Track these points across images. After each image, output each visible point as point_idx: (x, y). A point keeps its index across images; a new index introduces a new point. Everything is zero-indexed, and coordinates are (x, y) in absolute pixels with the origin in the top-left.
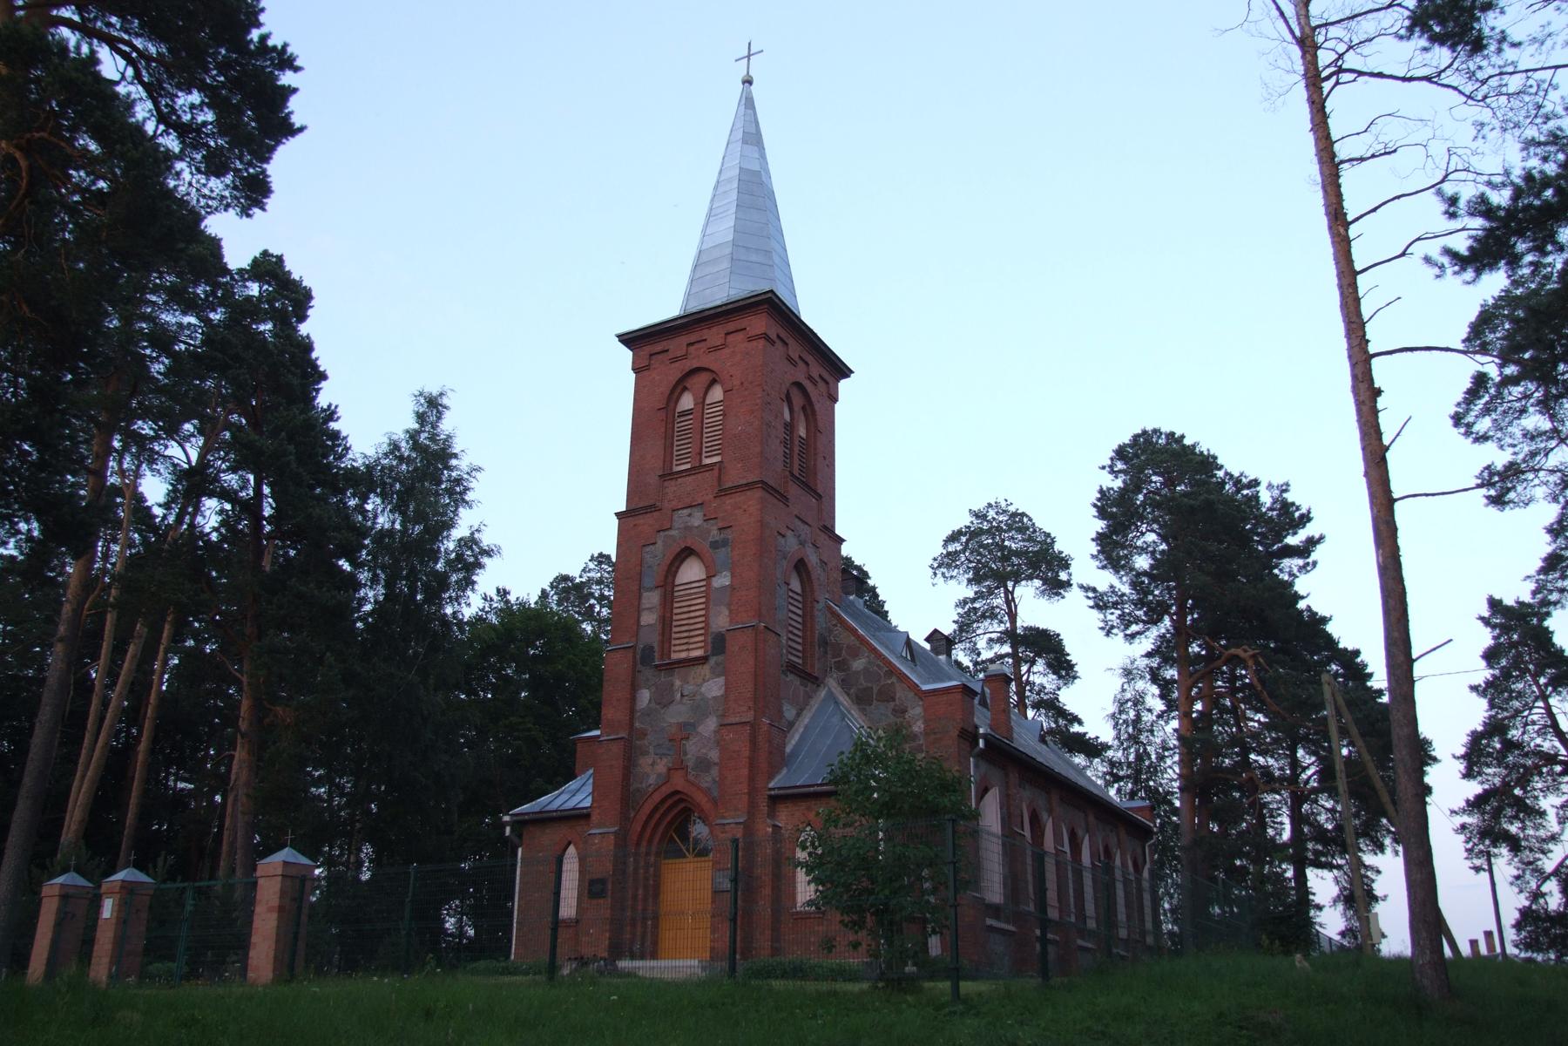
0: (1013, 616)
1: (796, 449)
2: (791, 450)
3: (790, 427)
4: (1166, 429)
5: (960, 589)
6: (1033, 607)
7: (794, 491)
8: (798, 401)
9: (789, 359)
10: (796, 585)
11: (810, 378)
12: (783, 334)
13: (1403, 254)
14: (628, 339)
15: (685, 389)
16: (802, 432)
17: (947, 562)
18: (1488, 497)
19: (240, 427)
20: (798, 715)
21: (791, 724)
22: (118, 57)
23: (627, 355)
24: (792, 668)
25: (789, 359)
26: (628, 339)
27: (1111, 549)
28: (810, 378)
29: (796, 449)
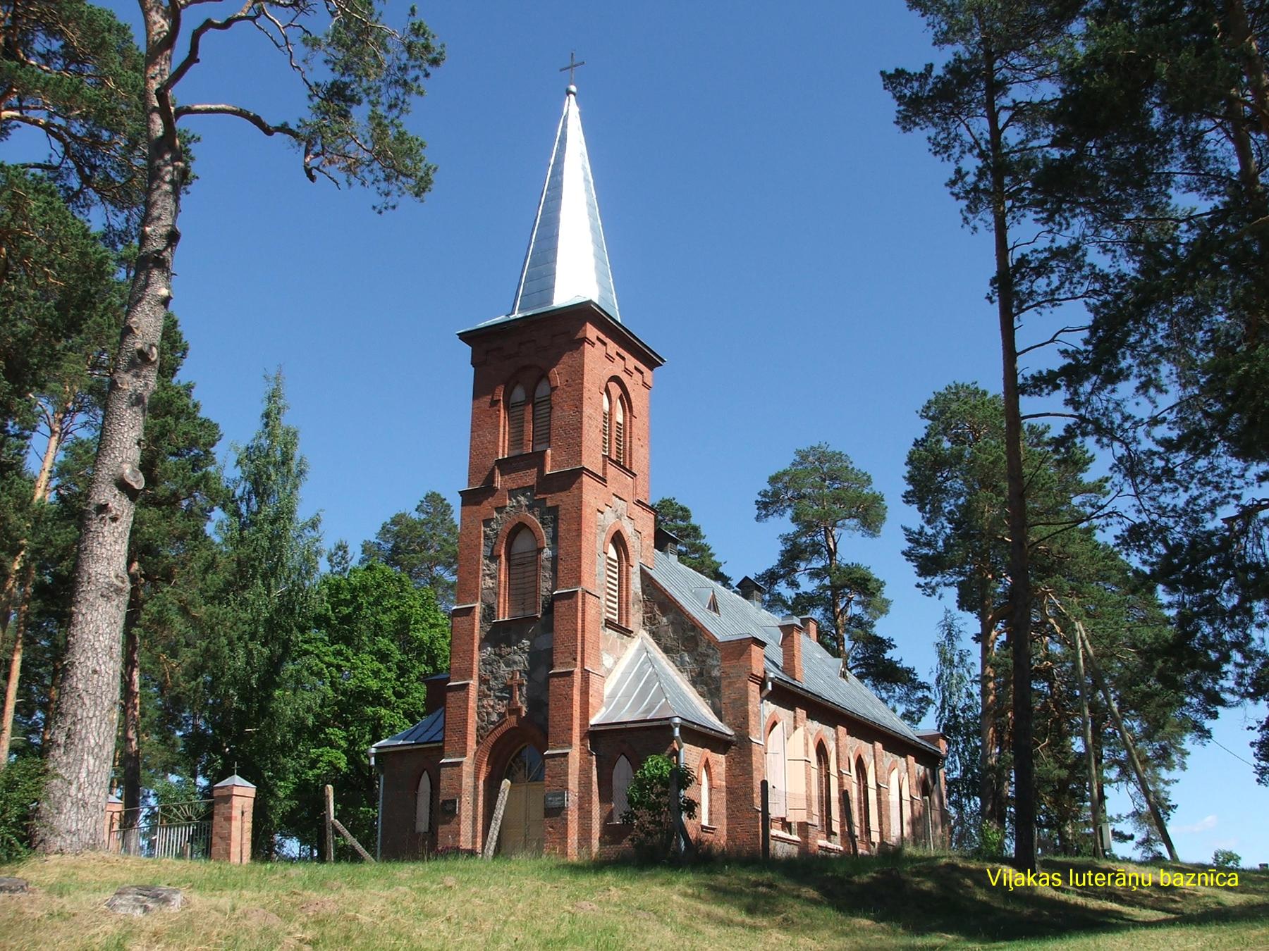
0: (832, 554)
1: (614, 435)
2: (610, 435)
3: (609, 416)
4: (910, 447)
5: (784, 524)
6: (852, 547)
7: (612, 471)
8: (615, 390)
9: (608, 356)
10: (612, 553)
11: (626, 370)
12: (602, 336)
13: (1052, 341)
14: (465, 337)
15: (517, 383)
16: (619, 417)
17: (768, 505)
18: (690, 817)
19: (31, 357)
20: (616, 663)
21: (609, 671)
22: (52, 138)
23: (467, 350)
24: (609, 624)
25: (608, 356)
26: (465, 337)
27: (924, 485)
28: (626, 370)
29: (614, 435)
